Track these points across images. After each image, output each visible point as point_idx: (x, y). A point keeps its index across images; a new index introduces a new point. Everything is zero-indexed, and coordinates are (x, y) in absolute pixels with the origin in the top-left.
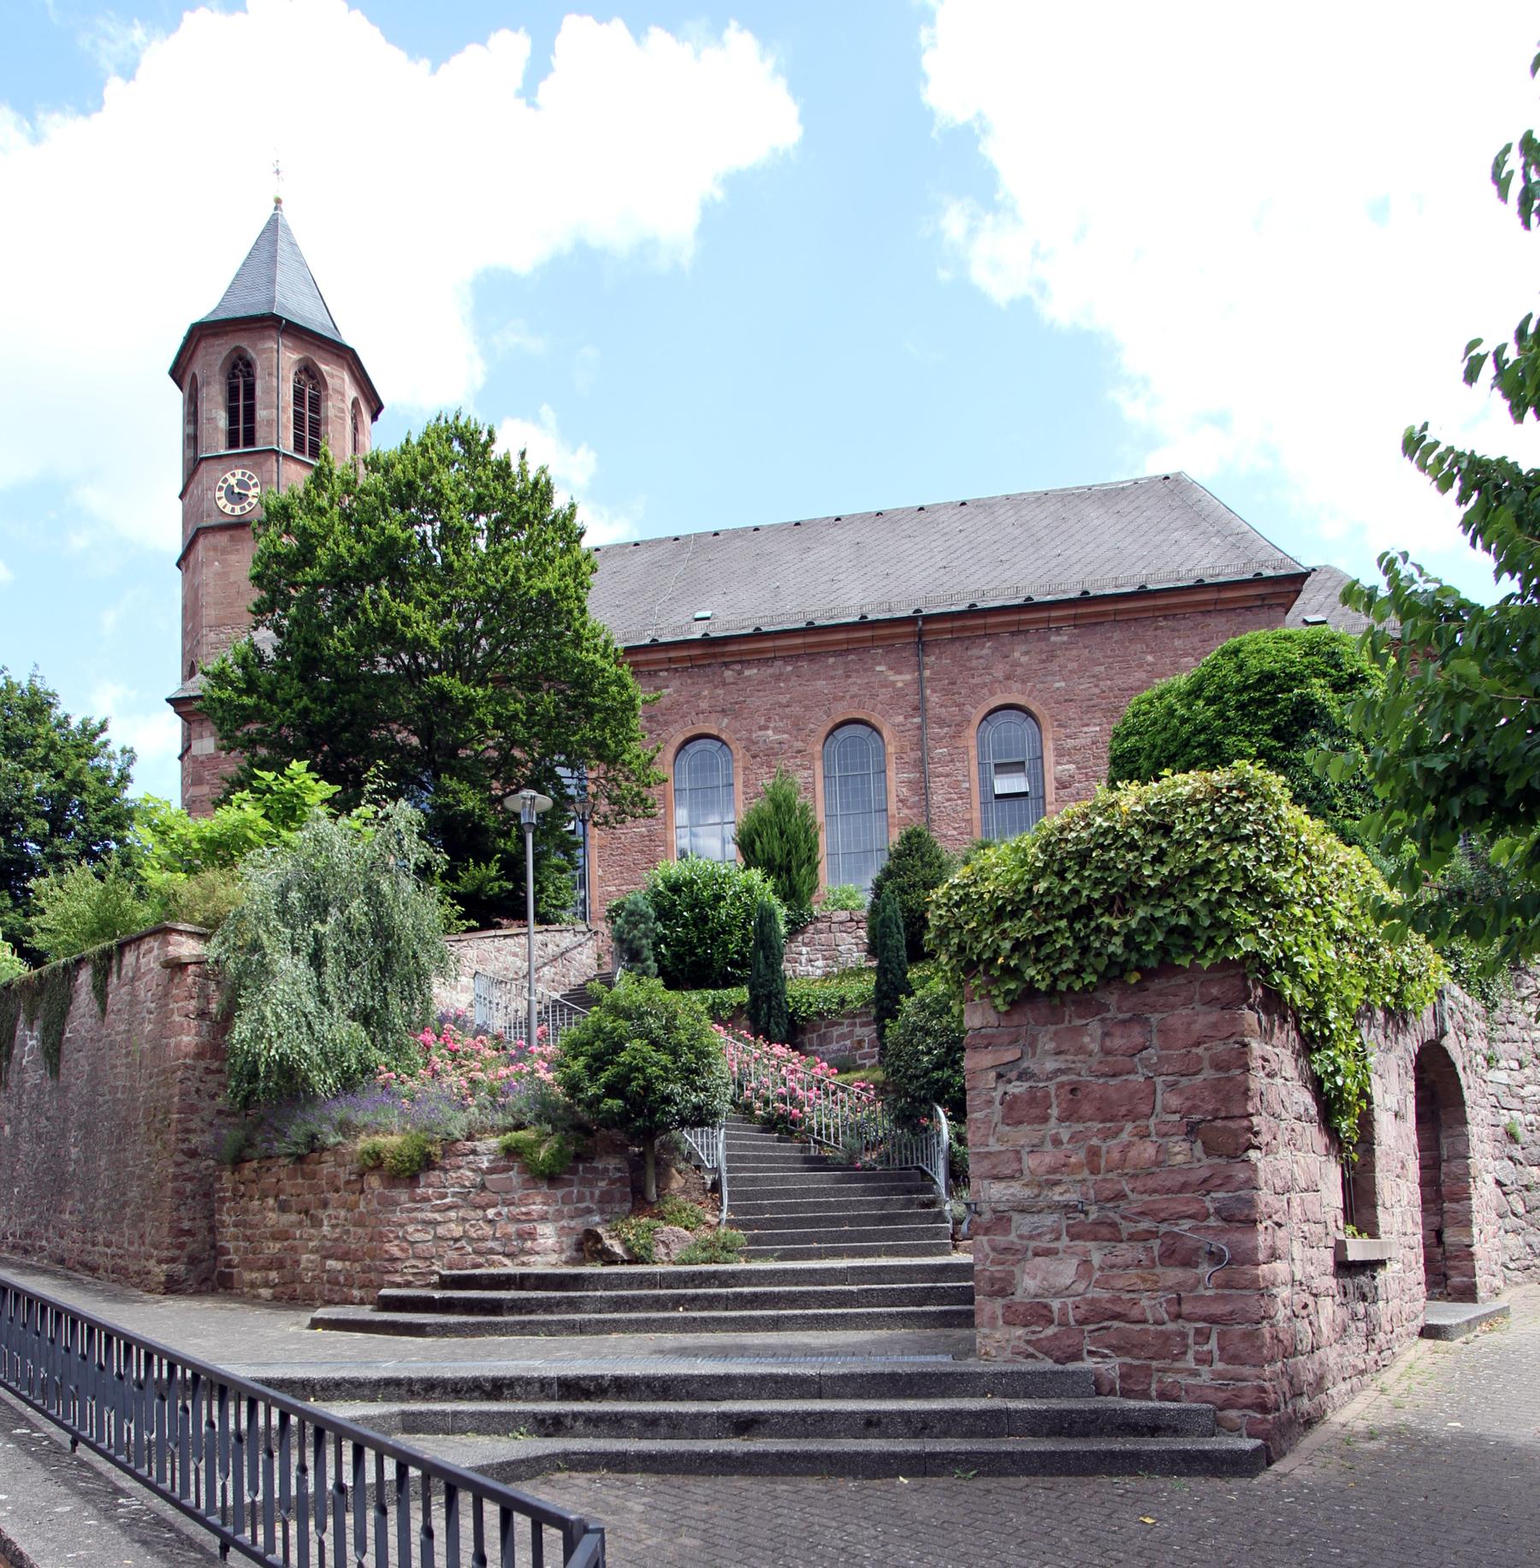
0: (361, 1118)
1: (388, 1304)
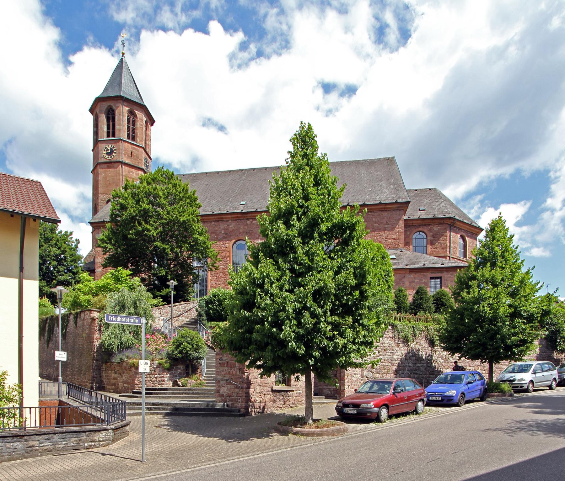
0: (131, 356)
1: (134, 393)
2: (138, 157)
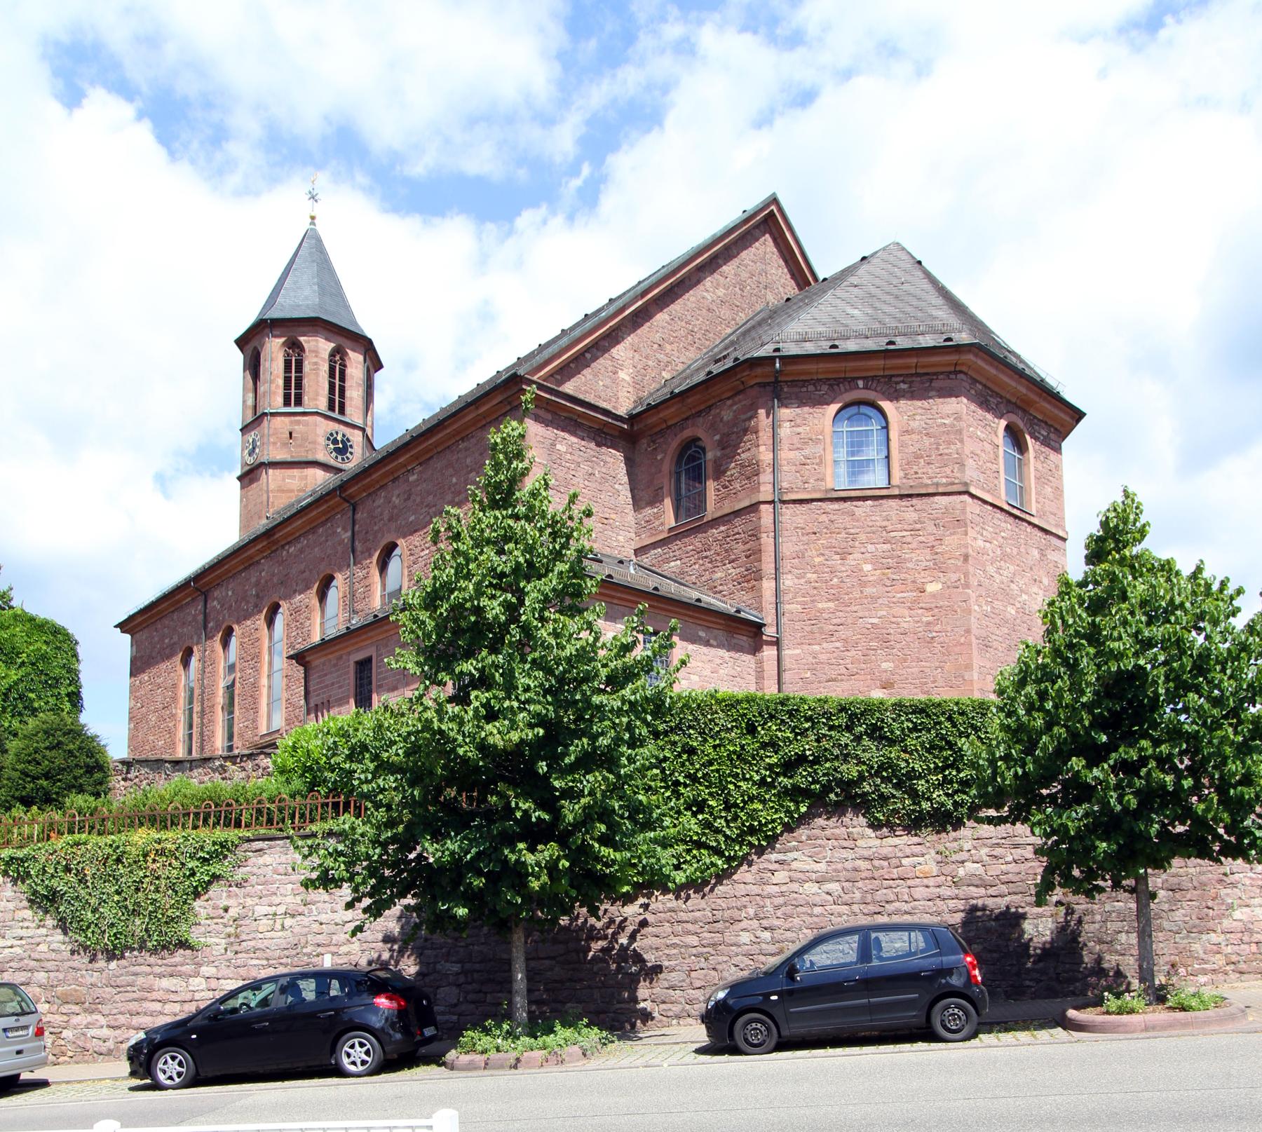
2: (305, 439)
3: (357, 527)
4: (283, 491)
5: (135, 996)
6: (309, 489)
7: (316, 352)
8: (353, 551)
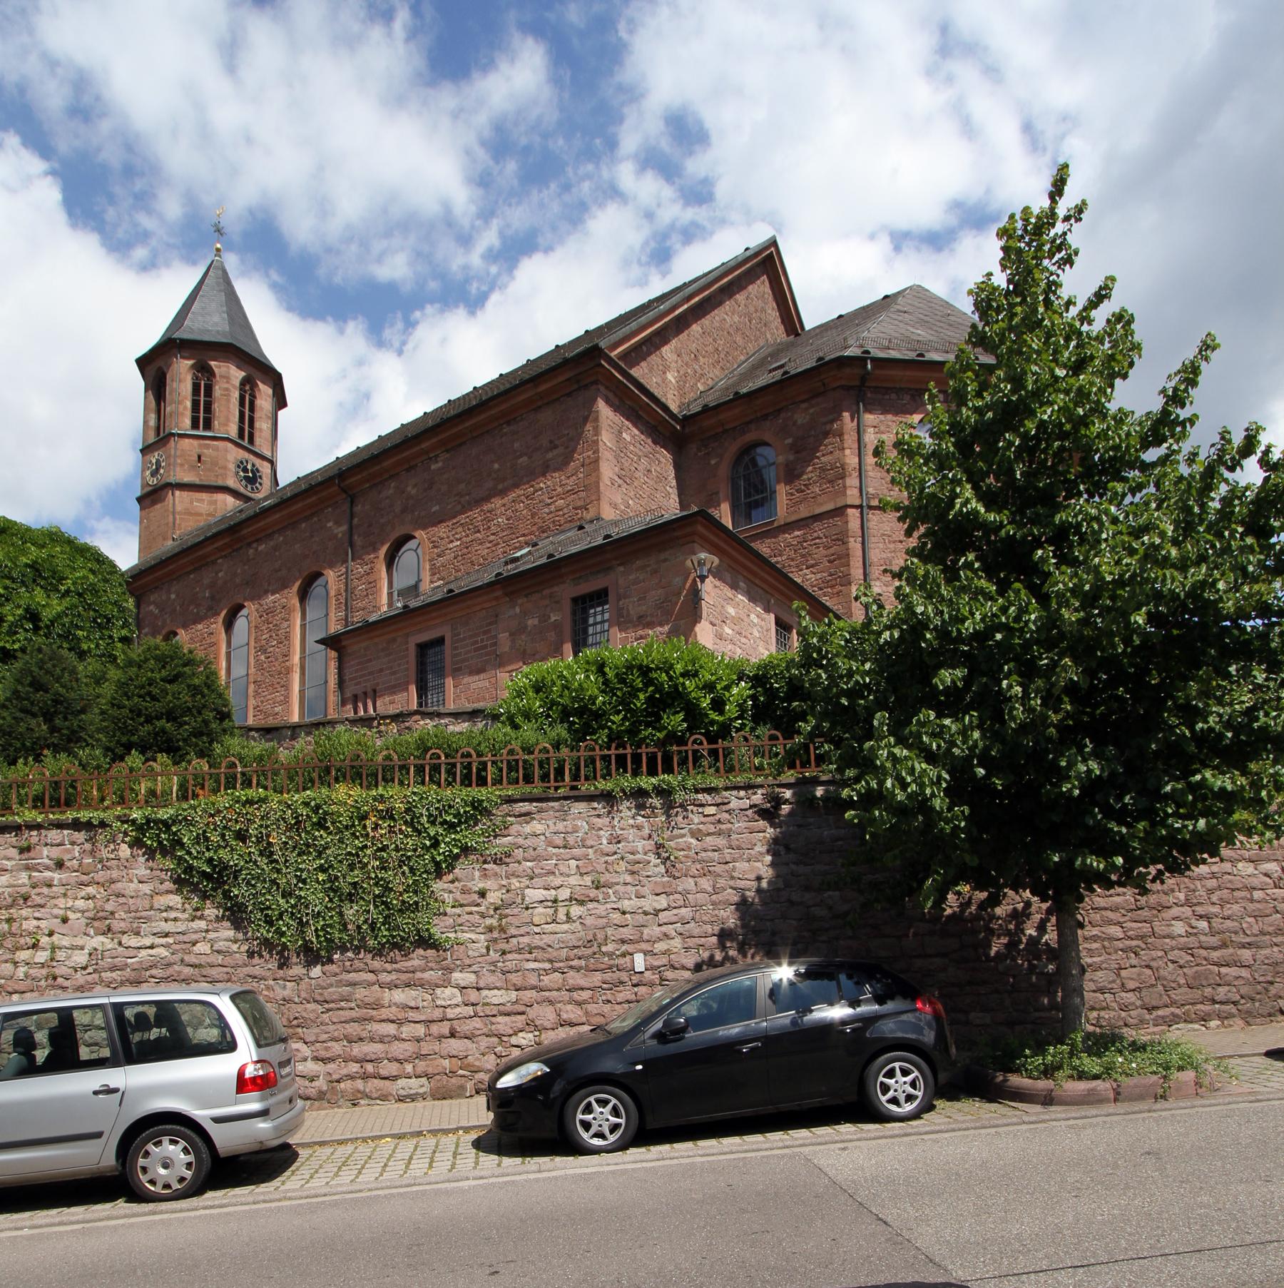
2: (214, 463)
3: (356, 521)
4: (191, 514)
5: (353, 1014)
6: (219, 515)
7: (227, 378)
8: (352, 545)
